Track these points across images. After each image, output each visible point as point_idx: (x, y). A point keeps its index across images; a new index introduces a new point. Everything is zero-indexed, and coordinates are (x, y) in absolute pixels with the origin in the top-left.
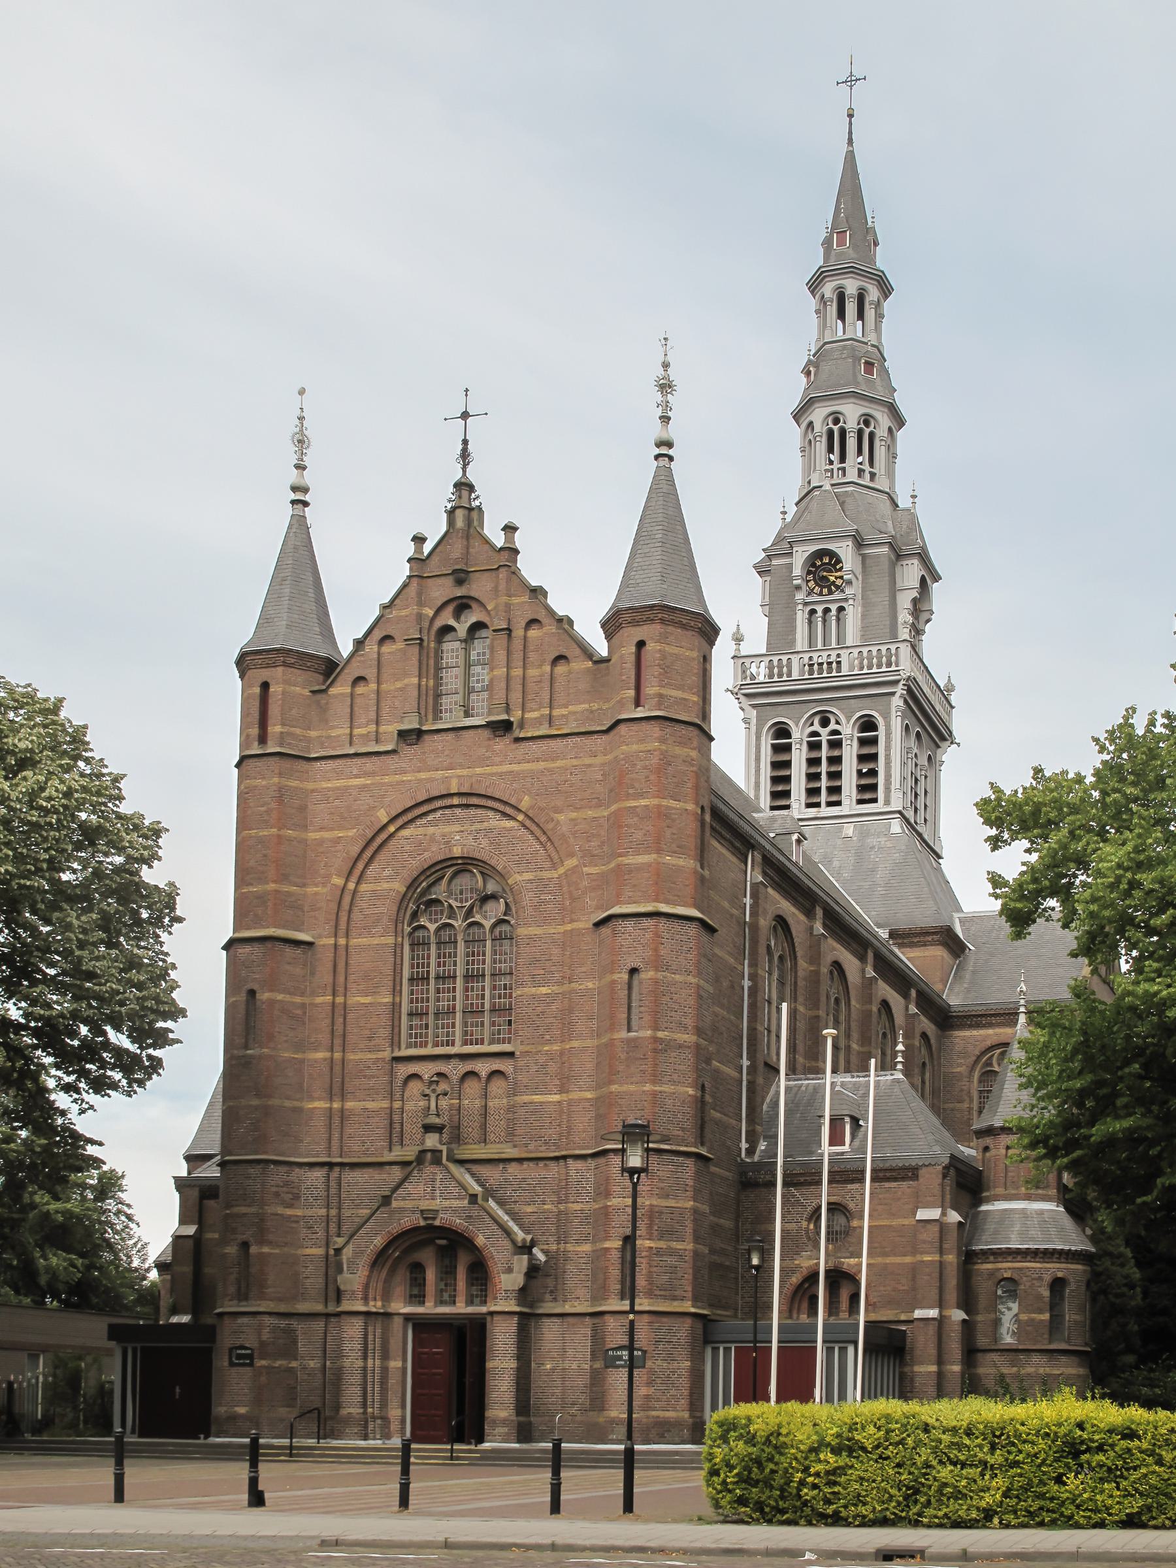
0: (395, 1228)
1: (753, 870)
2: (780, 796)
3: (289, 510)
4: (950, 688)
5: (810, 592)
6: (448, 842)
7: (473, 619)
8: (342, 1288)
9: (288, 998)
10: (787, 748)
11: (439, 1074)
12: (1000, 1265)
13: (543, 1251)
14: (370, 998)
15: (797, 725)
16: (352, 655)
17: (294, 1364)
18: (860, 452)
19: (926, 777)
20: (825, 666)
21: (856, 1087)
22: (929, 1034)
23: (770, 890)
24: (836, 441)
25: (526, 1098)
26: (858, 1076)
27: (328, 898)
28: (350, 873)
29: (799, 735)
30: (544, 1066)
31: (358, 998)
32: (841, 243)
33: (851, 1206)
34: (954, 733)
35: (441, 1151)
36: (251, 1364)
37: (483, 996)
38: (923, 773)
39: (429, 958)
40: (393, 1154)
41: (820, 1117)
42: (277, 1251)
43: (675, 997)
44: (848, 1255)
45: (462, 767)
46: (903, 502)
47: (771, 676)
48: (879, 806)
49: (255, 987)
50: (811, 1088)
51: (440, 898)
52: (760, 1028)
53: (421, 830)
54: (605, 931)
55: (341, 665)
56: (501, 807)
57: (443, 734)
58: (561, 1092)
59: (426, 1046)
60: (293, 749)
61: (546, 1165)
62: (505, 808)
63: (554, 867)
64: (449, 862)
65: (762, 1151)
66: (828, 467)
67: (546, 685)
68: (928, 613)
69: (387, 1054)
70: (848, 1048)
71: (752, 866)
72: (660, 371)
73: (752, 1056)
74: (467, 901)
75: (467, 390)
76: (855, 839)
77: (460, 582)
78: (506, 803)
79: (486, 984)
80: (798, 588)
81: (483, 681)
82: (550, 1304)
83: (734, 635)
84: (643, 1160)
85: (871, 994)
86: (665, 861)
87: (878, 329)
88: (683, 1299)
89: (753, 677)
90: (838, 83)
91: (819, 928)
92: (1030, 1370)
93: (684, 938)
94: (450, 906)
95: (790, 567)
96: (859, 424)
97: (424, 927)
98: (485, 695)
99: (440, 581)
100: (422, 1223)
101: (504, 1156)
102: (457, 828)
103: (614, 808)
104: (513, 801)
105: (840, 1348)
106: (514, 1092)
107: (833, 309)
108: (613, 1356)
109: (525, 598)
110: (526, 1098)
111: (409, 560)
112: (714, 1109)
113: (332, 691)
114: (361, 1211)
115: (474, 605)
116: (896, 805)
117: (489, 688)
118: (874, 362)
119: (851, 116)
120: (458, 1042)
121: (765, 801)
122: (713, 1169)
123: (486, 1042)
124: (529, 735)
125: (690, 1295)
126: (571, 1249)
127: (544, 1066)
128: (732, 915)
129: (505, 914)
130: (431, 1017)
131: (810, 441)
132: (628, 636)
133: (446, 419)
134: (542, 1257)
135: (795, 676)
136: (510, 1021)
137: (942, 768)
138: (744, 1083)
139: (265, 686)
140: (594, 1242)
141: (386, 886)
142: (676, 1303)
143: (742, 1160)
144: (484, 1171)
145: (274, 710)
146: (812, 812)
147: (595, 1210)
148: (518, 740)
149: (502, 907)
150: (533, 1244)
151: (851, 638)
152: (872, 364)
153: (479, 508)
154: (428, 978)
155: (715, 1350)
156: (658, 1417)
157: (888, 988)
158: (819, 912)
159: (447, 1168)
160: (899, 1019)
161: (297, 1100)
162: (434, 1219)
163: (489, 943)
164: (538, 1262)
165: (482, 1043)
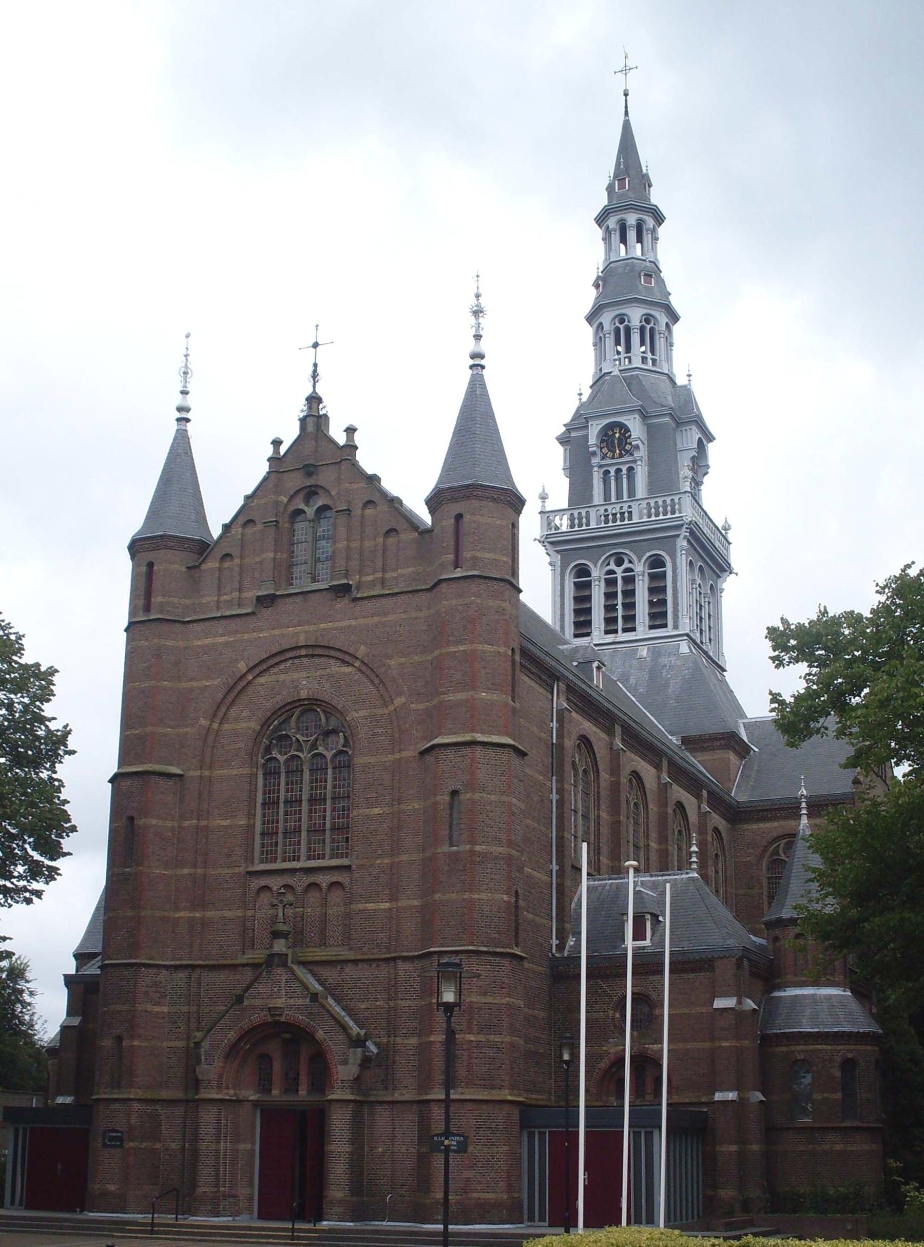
0: (246, 1024)
1: (558, 698)
2: (583, 626)
3: (174, 426)
4: (727, 528)
6: (296, 687)
7: (320, 503)
8: (200, 1077)
9: (160, 823)
10: (588, 585)
12: (793, 1048)
13: (375, 1043)
15: (595, 566)
18: (642, 343)
19: (709, 603)
20: (618, 515)
22: (720, 828)
23: (574, 714)
24: (623, 336)
25: (361, 906)
26: (656, 876)
27: (197, 737)
28: (215, 715)
29: (597, 573)
32: (622, 186)
33: (654, 996)
34: (732, 565)
35: (287, 955)
36: (121, 1146)
37: (325, 817)
38: (707, 600)
40: (246, 957)
43: (491, 814)
45: (308, 623)
46: (681, 380)
47: (572, 526)
48: (669, 631)
49: (135, 814)
51: (289, 733)
52: (566, 835)
53: (274, 678)
54: (429, 758)
55: (212, 545)
56: (341, 656)
57: (294, 597)
58: (391, 900)
60: (171, 615)
61: (378, 966)
62: (345, 657)
63: (385, 705)
64: (297, 703)
65: (571, 947)
66: (616, 357)
69: (242, 870)
70: (647, 846)
71: (558, 695)
72: (474, 301)
75: (317, 326)
77: (309, 474)
78: (345, 652)
79: (327, 806)
80: (594, 453)
81: (327, 552)
82: (382, 1092)
84: (455, 995)
86: (481, 697)
87: (654, 248)
88: (501, 1088)
89: (557, 528)
90: (615, 72)
91: (619, 743)
92: (827, 1147)
94: (298, 740)
95: (586, 437)
96: (641, 322)
97: (275, 759)
98: (329, 563)
99: (293, 474)
101: (341, 958)
102: (304, 674)
103: (436, 653)
104: (351, 651)
106: (349, 900)
107: (616, 237)
108: (438, 1141)
110: (361, 906)
111: (269, 460)
112: (528, 912)
113: (204, 567)
115: (320, 491)
117: (332, 558)
118: (653, 272)
119: (626, 95)
120: (303, 858)
121: (569, 630)
123: (327, 856)
124: (365, 595)
126: (400, 1042)
127: (377, 878)
128: (540, 739)
129: (343, 746)
130: (280, 836)
131: (601, 338)
135: (593, 525)
136: (347, 838)
137: (722, 595)
138: (554, 886)
139: (151, 565)
141: (244, 725)
142: (494, 1092)
143: (553, 955)
145: (156, 584)
146: (610, 638)
147: (421, 1006)
148: (355, 600)
149: (342, 740)
150: (367, 1037)
152: (651, 276)
153: (326, 416)
154: (278, 803)
155: (531, 1136)
156: (479, 1199)
157: (681, 790)
158: (618, 730)
159: (293, 972)
160: (693, 817)
163: (330, 771)
164: (371, 1054)
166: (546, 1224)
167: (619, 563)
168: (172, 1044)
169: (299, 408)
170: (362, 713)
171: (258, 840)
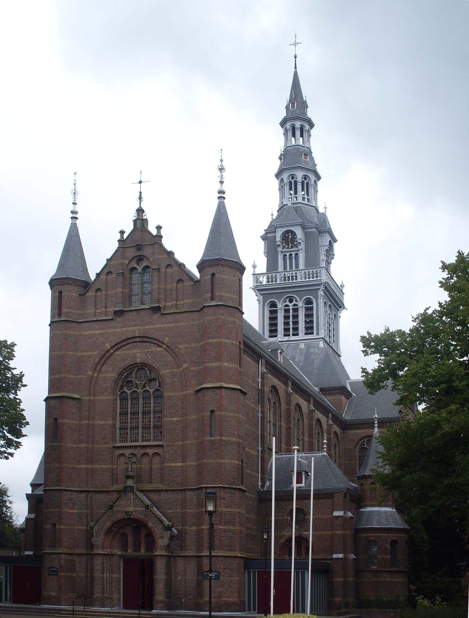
0: (115, 519)
2: (273, 332)
4: (342, 286)
5: (284, 248)
6: (135, 357)
7: (144, 265)
8: (93, 543)
9: (70, 422)
10: (276, 312)
11: (132, 454)
12: (369, 535)
13: (176, 529)
14: (103, 422)
15: (279, 302)
16: (95, 280)
17: (74, 575)
18: (303, 190)
20: (291, 277)
21: (306, 459)
23: (269, 375)
24: (293, 185)
28: (95, 370)
29: (280, 306)
30: (176, 451)
31: (99, 422)
32: (293, 107)
33: (306, 509)
34: (345, 305)
36: (57, 575)
37: (150, 421)
38: (332, 321)
39: (127, 405)
41: (292, 471)
42: (67, 527)
44: (305, 530)
45: (140, 326)
46: (321, 210)
47: (268, 282)
48: (314, 336)
49: (57, 417)
50: (288, 458)
51: (132, 380)
53: (124, 352)
54: (200, 394)
55: (91, 284)
56: (156, 342)
57: (132, 312)
58: (183, 462)
59: (127, 442)
61: (177, 493)
62: (159, 343)
63: (178, 367)
64: (135, 365)
65: (268, 486)
66: (290, 196)
67: (174, 292)
68: (333, 255)
72: (219, 163)
73: (262, 446)
74: (143, 381)
76: (304, 349)
77: (139, 250)
78: (158, 341)
80: (279, 245)
81: (149, 290)
83: (253, 265)
85: (313, 417)
86: (224, 365)
87: (309, 141)
89: (261, 282)
90: (290, 45)
93: (233, 397)
94: (136, 383)
96: (302, 179)
98: (149, 296)
100: (126, 517)
103: (203, 343)
104: (161, 340)
105: (301, 572)
106: (163, 462)
107: (290, 133)
109: (165, 256)
110: (168, 465)
113: (87, 295)
114: (101, 511)
115: (144, 259)
116: (322, 334)
117: (151, 293)
118: (308, 153)
119: (295, 57)
120: (140, 440)
121: (267, 334)
122: (247, 494)
123: (152, 440)
124: (168, 312)
125: (238, 549)
126: (188, 528)
127: (176, 451)
128: (253, 386)
129: (159, 387)
130: (129, 430)
132: (208, 272)
133: (133, 184)
134: (176, 532)
135: (278, 282)
136: (161, 432)
137: (340, 319)
138: (260, 457)
139: (61, 293)
140: (197, 526)
141: (109, 375)
142: (232, 552)
143: (259, 490)
144: (152, 495)
145: (64, 302)
146: (286, 338)
147: (198, 512)
148: (163, 314)
149: (158, 384)
151: (301, 266)
152: (307, 155)
154: (127, 414)
155: (249, 572)
157: (320, 414)
159: (136, 494)
160: (325, 427)
161: (74, 464)
162: (131, 515)
163: (152, 399)
164: (174, 534)
165: (150, 441)
166: (256, 612)
167: (291, 301)
168: (80, 528)
169: (133, 215)
170: (167, 371)
171: (118, 431)
